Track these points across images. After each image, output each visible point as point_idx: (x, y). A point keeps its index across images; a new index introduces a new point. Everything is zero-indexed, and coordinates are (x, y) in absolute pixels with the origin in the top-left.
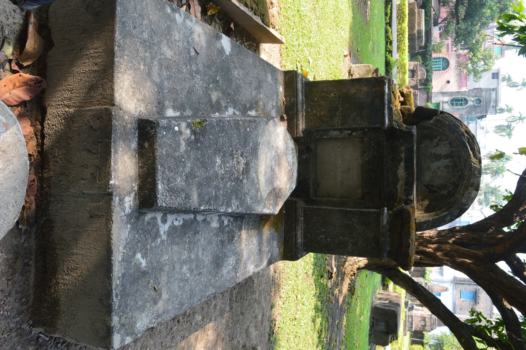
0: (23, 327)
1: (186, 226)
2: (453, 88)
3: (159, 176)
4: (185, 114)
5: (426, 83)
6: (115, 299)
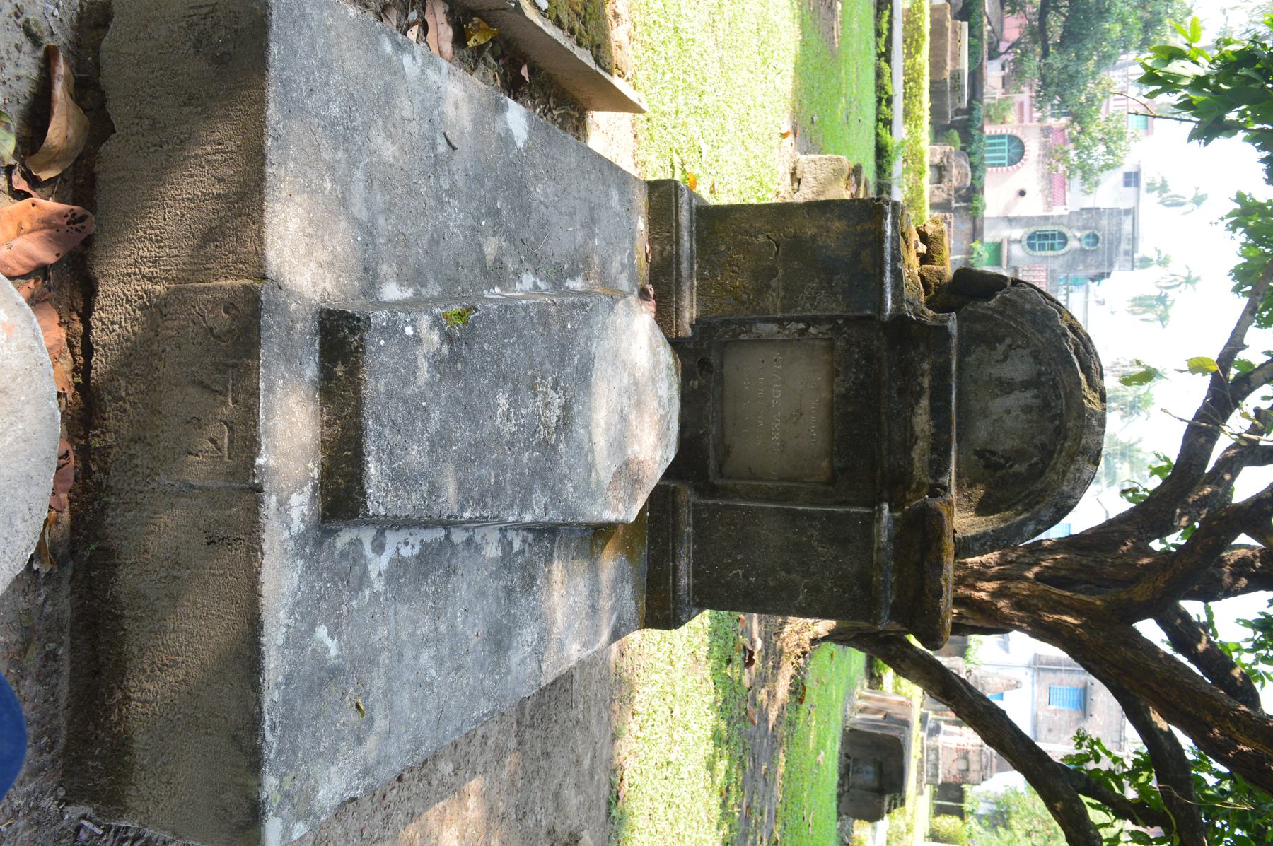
0: (43, 804)
1: (428, 556)
2: (1033, 206)
3: (371, 445)
4: (424, 292)
5: (970, 195)
6: (269, 737)
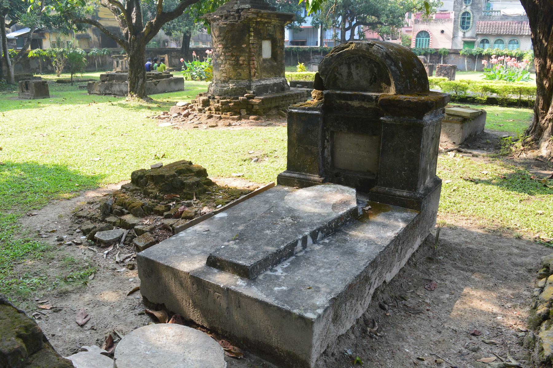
2: (449, 27)
